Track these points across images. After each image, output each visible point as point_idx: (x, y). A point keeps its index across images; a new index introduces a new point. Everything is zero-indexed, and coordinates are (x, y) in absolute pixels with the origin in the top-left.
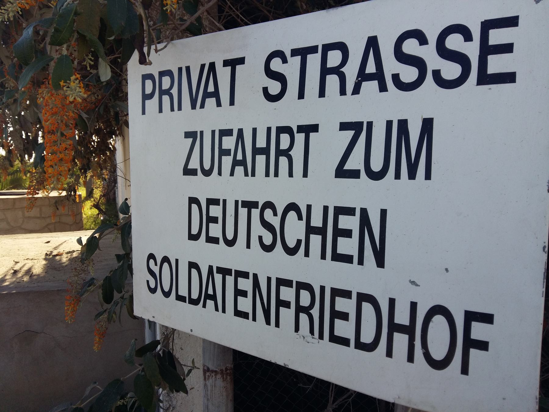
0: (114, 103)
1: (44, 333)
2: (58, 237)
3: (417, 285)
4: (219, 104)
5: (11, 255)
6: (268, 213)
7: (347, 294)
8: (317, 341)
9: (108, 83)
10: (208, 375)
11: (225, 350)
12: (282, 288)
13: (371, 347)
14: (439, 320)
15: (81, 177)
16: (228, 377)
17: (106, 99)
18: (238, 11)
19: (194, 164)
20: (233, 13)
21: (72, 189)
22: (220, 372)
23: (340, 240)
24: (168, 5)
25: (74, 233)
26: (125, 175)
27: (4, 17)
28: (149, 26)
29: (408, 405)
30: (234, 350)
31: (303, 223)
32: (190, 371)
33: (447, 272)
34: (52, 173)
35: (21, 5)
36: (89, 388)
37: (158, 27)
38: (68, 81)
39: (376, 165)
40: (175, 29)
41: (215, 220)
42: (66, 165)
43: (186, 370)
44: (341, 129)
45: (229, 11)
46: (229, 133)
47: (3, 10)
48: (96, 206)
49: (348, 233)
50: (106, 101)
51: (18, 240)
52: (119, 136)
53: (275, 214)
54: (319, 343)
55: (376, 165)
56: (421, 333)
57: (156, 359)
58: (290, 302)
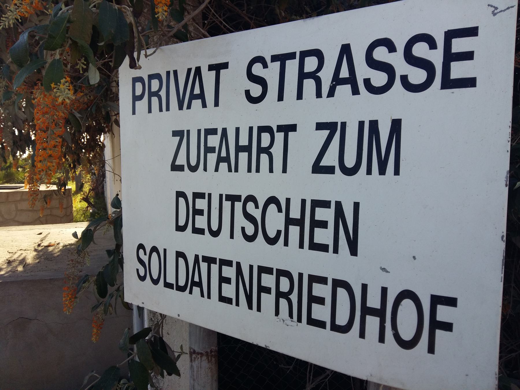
0: (105, 104)
1: (37, 320)
2: (50, 229)
3: (387, 272)
4: (204, 105)
5: (6, 246)
6: (250, 206)
7: (323, 280)
8: (296, 324)
9: (100, 84)
10: (194, 357)
11: (209, 333)
12: (263, 275)
13: (345, 329)
14: (407, 304)
15: (70, 172)
16: (213, 358)
17: (98, 99)
18: (221, 17)
19: (181, 160)
20: (217, 19)
21: (62, 184)
22: (206, 354)
23: (317, 230)
24: (160, 12)
25: (65, 226)
26: (114, 170)
27: (5, 24)
28: (138, 32)
29: (379, 382)
30: (218, 334)
31: (283, 215)
32: (179, 356)
33: (415, 260)
34: (41, 168)
35: (21, 13)
36: (87, 377)
37: (147, 33)
38: (59, 84)
39: (350, 162)
40: (164, 35)
41: (200, 212)
42: (55, 161)
43: (176, 354)
44: (317, 129)
45: (212, 18)
46: (213, 131)
47: (4, 18)
48: (86, 199)
49: (324, 224)
50: (98, 102)
51: (11, 231)
52: (107, 133)
53: (257, 207)
54: (297, 325)
55: (350, 162)
56: (391, 315)
57: (148, 345)
58: (270, 288)
